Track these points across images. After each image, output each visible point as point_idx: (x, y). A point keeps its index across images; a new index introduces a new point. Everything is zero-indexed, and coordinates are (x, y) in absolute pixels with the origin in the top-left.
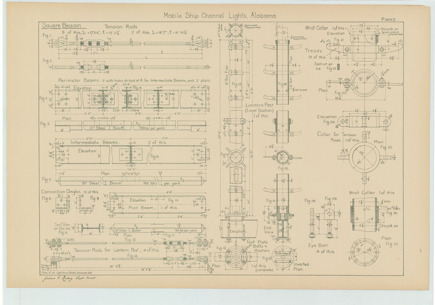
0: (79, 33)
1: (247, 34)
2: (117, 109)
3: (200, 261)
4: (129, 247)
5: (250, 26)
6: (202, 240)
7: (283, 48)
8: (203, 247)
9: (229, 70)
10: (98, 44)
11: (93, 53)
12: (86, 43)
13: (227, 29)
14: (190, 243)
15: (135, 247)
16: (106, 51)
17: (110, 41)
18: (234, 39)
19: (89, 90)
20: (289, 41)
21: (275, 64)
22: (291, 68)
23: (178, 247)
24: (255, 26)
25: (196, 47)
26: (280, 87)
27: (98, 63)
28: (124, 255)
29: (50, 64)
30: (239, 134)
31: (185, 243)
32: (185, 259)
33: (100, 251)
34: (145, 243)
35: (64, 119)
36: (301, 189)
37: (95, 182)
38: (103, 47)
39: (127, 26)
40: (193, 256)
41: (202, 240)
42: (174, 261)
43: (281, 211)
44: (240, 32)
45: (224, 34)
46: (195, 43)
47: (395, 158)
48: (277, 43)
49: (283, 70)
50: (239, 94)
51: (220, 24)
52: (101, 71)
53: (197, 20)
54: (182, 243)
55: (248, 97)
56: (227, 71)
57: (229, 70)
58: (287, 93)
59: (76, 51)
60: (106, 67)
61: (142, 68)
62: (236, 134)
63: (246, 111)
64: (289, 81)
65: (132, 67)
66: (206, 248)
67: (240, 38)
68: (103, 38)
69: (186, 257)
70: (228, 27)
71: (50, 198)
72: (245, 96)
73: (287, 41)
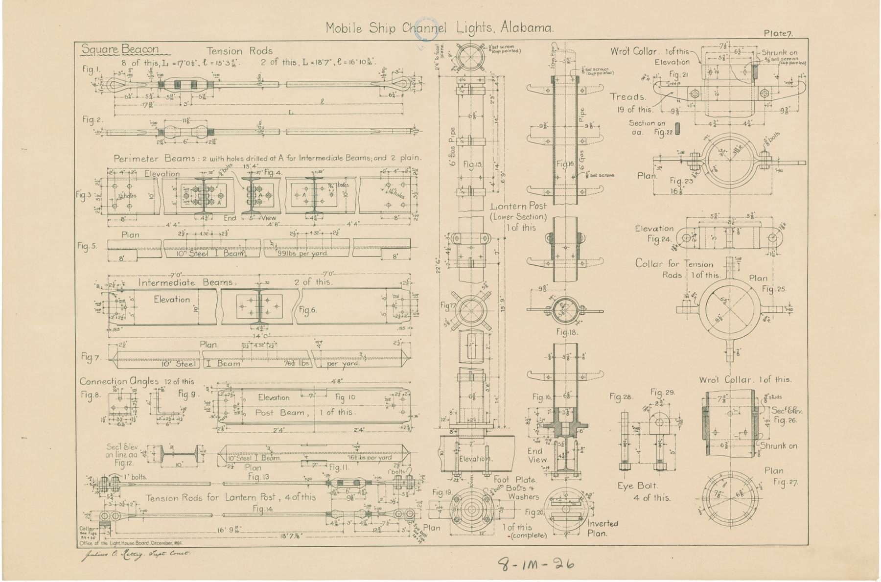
0: (156, 64)
3: (399, 518)
4: (256, 491)
5: (499, 49)
6: (404, 477)
8: (404, 490)
10: (194, 85)
11: (183, 104)
12: (170, 85)
13: (454, 54)
14: (380, 483)
15: (269, 491)
16: (209, 100)
17: (217, 79)
18: (468, 74)
20: (578, 78)
21: (550, 124)
22: (583, 132)
23: (354, 490)
27: (192, 124)
28: (246, 506)
29: (97, 126)
30: (478, 263)
31: (369, 483)
32: (369, 514)
33: (197, 499)
34: (289, 483)
39: (252, 50)
40: (385, 508)
42: (346, 519)
44: (478, 60)
45: (446, 64)
48: (553, 82)
49: (565, 136)
50: (477, 184)
53: (393, 36)
54: (362, 483)
56: (454, 139)
57: (457, 136)
58: (574, 181)
59: (149, 100)
60: (211, 132)
61: (283, 134)
62: (471, 265)
63: (492, 217)
65: (261, 131)
66: (412, 491)
67: (479, 72)
68: (204, 74)
69: (372, 510)
70: (455, 51)
72: (489, 188)
73: (574, 78)
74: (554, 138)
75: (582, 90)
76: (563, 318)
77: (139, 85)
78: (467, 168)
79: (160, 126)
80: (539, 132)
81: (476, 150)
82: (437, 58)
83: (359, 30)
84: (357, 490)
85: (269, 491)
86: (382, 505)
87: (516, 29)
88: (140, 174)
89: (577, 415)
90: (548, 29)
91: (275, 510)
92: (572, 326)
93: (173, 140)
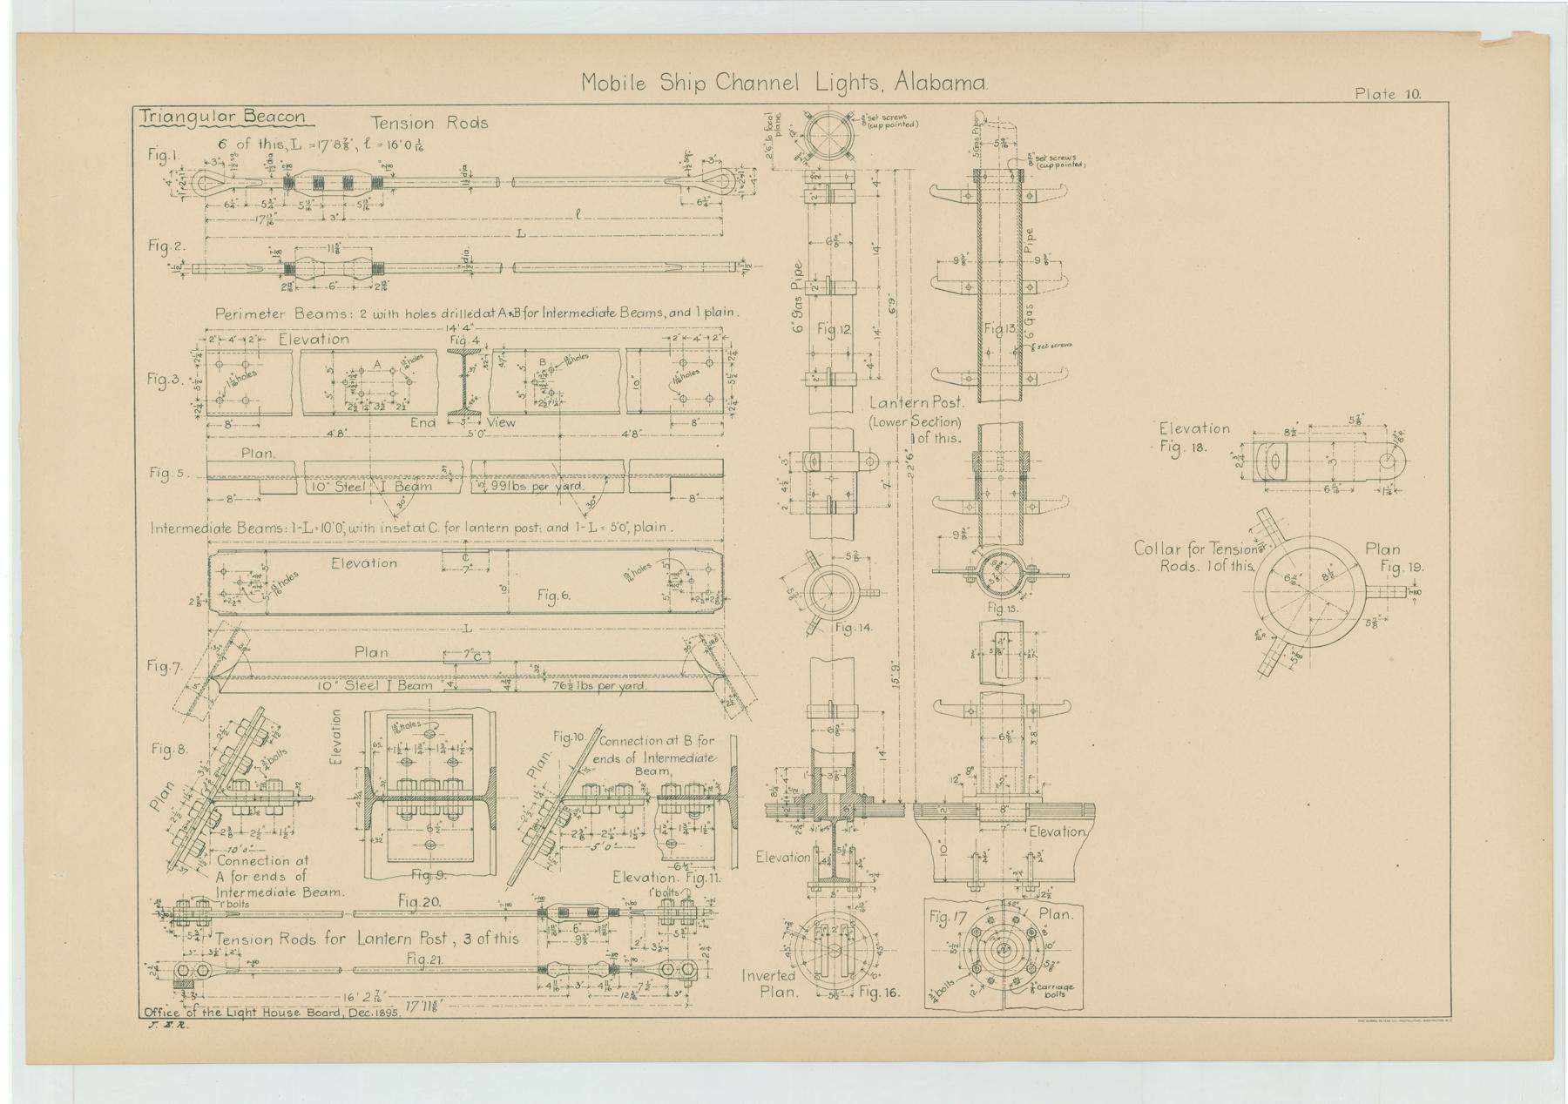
1: (873, 148)
3: (669, 976)
4: (411, 927)
6: (678, 903)
7: (999, 193)
8: (678, 926)
9: (805, 278)
10: (348, 183)
11: (328, 217)
12: (305, 183)
13: (800, 130)
15: (435, 927)
16: (374, 211)
17: (389, 174)
18: (825, 165)
20: (1021, 171)
21: (973, 257)
22: (1031, 271)
23: (589, 926)
25: (702, 195)
26: (989, 339)
27: (345, 255)
28: (395, 955)
30: (844, 506)
31: (614, 913)
32: (613, 970)
34: (470, 914)
35: (247, 457)
37: (368, 682)
39: (451, 120)
40: (650, 959)
41: (678, 903)
42: (574, 979)
44: (843, 142)
45: (786, 148)
47: (1416, 592)
49: (1000, 277)
50: (841, 365)
51: (775, 110)
52: (357, 283)
54: (603, 912)
55: (875, 376)
58: (1014, 360)
59: (267, 211)
60: (378, 269)
61: (507, 272)
62: (833, 508)
65: (467, 266)
66: (692, 929)
67: (844, 162)
68: (364, 165)
69: (619, 962)
70: (801, 125)
72: (863, 372)
73: (1015, 173)
77: (249, 183)
79: (287, 258)
81: (841, 304)
82: (770, 138)
84: (594, 926)
85: (435, 927)
86: (636, 953)
87: (922, 84)
88: (271, 341)
89: (854, 779)
93: (311, 283)
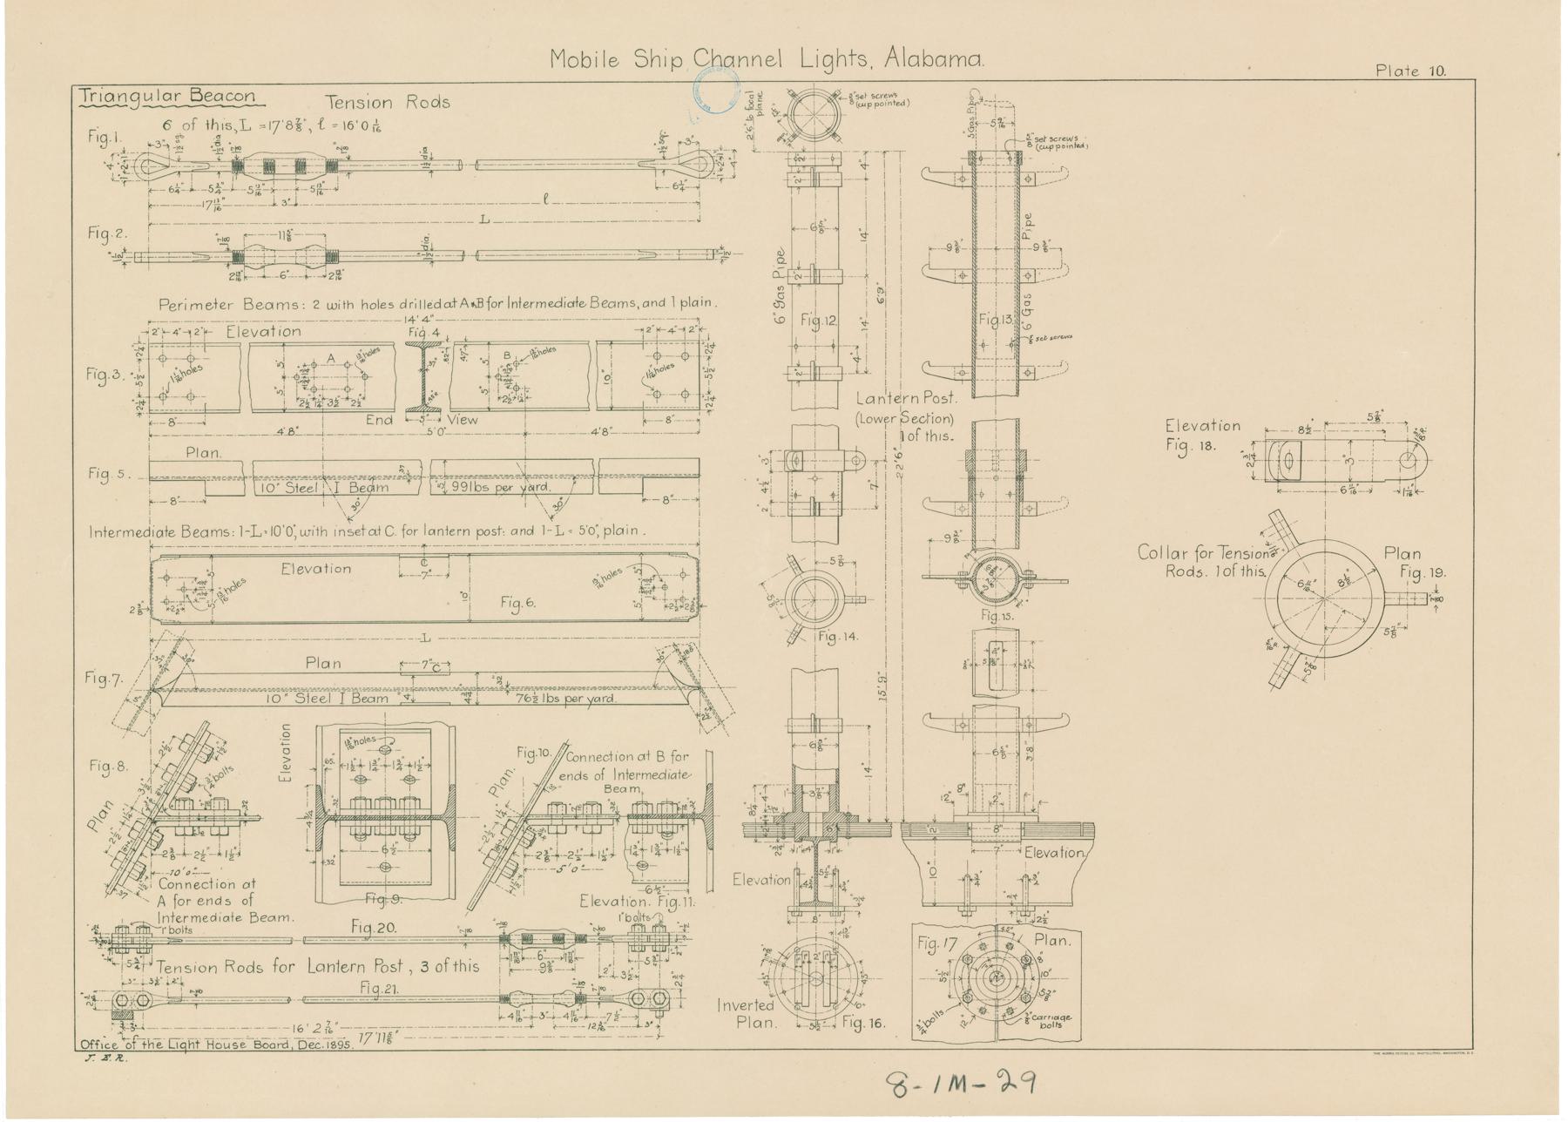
0: (228, 126)
2: (385, 416)
4: (365, 954)
5: (869, 99)
6: (649, 929)
7: (996, 177)
8: (649, 952)
9: (788, 266)
10: (300, 166)
11: (279, 202)
12: (254, 167)
14: (604, 939)
15: (390, 954)
16: (328, 196)
17: (344, 156)
18: (810, 146)
19: (285, 338)
20: (1019, 154)
21: (967, 244)
23: (554, 953)
24: (894, 100)
25: (678, 178)
27: (298, 242)
28: (348, 984)
29: (116, 246)
30: (828, 508)
31: (581, 939)
32: (580, 999)
33: (255, 968)
34: (428, 940)
36: (1064, 721)
38: (320, 181)
39: (411, 99)
42: (538, 1009)
43: (809, 803)
45: (768, 128)
46: (669, 165)
47: (1438, 599)
48: (973, 163)
50: (826, 358)
52: (310, 273)
54: (569, 938)
55: (862, 370)
56: (783, 273)
57: (788, 266)
58: (1011, 353)
59: (214, 196)
60: (332, 257)
61: (470, 260)
62: (816, 509)
63: (860, 420)
64: (1021, 309)
65: (427, 254)
66: (664, 956)
67: (830, 143)
69: (586, 991)
70: (784, 104)
71: (121, 765)
72: (849, 366)
73: (1013, 155)
74: (975, 268)
75: (1028, 179)
76: (990, 593)
77: (196, 166)
78: (807, 328)
79: (236, 245)
80: (943, 259)
81: (827, 294)
82: (751, 118)
83: (612, 61)
84: (561, 953)
85: (390, 954)
88: (218, 334)
90: (974, 60)
91: (401, 991)
92: (1010, 607)
93: (261, 273)
